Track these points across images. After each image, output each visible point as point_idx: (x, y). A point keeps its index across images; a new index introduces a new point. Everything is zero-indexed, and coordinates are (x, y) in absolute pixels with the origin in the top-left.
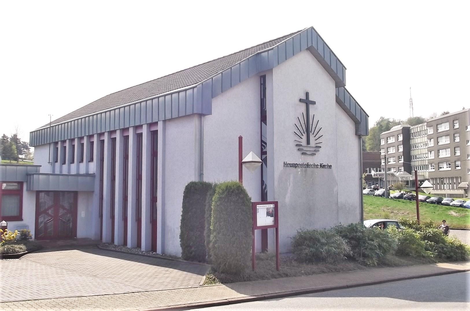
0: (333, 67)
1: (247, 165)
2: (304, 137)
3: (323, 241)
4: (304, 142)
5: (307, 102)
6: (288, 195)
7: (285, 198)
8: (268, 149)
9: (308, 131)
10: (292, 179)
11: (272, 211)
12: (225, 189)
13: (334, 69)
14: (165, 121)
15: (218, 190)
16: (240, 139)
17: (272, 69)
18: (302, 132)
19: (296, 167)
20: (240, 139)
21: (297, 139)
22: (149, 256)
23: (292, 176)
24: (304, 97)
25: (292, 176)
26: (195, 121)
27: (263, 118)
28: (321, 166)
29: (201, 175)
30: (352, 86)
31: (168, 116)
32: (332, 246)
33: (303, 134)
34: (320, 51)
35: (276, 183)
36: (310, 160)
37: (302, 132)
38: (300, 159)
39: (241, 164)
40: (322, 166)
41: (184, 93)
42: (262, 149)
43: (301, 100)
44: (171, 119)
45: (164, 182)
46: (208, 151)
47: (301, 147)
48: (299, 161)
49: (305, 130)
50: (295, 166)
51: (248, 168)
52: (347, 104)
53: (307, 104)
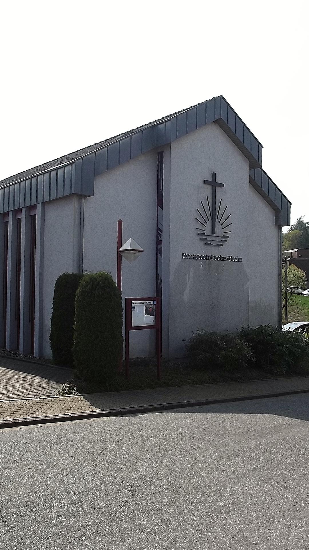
0: (247, 144)
1: (126, 254)
2: (209, 225)
3: (221, 345)
4: (208, 230)
5: (213, 184)
6: (187, 291)
7: (183, 295)
8: (164, 239)
9: (213, 218)
10: (191, 273)
11: (153, 309)
12: (89, 281)
13: (248, 147)
14: (44, 204)
15: (82, 282)
16: (120, 223)
17: (170, 144)
18: (206, 219)
19: (197, 259)
20: (120, 223)
21: (200, 226)
22: (20, 360)
23: (192, 270)
24: (210, 179)
25: (192, 270)
26: (74, 203)
27: (160, 203)
28: (228, 259)
29: (80, 265)
30: (269, 165)
31: (47, 199)
32: (231, 351)
33: (207, 221)
34: (231, 125)
35: (172, 277)
36: (215, 252)
37: (206, 219)
38: (202, 250)
39: (120, 253)
40: (230, 259)
41: (62, 170)
42: (157, 238)
43: (205, 182)
44: (50, 202)
45: (41, 275)
46: (98, 239)
47: (204, 237)
48: (202, 253)
49: (209, 217)
50: (198, 258)
51: (126, 258)
52: (265, 189)
53: (213, 186)
